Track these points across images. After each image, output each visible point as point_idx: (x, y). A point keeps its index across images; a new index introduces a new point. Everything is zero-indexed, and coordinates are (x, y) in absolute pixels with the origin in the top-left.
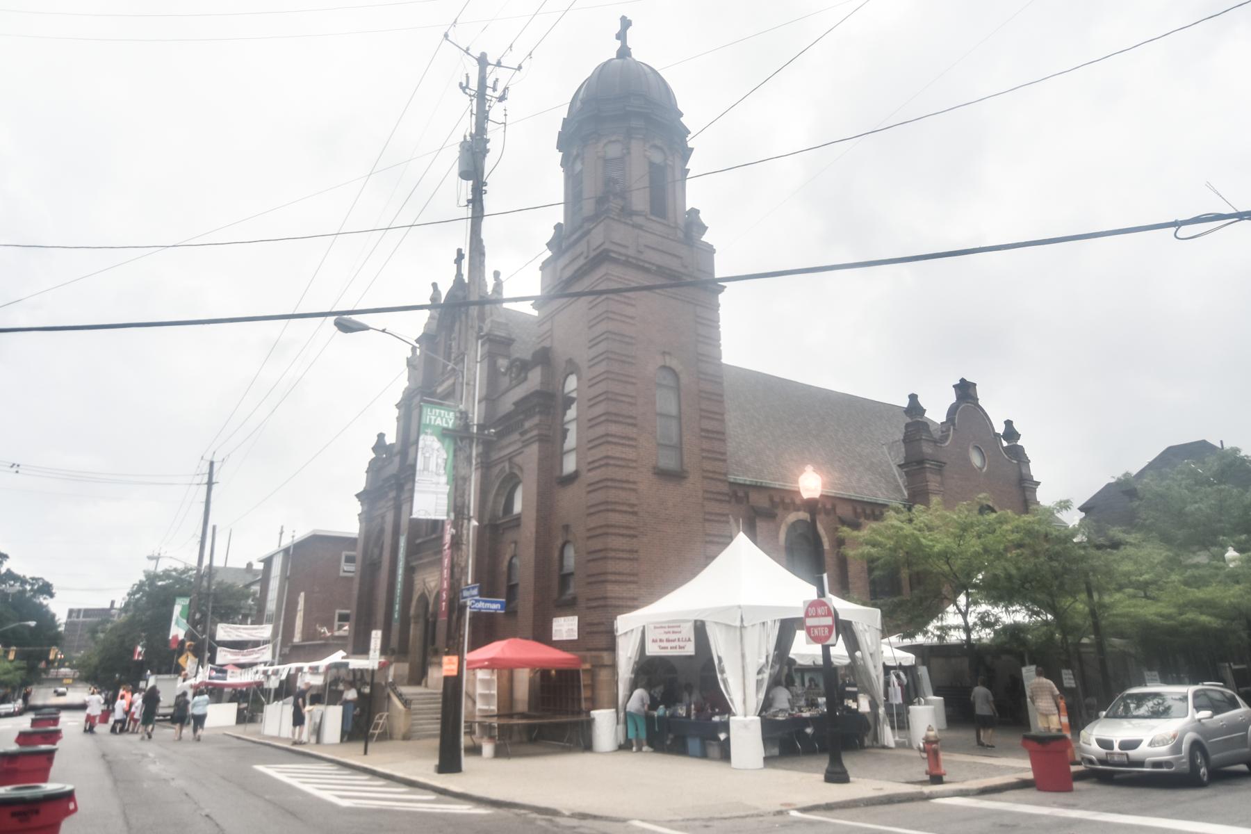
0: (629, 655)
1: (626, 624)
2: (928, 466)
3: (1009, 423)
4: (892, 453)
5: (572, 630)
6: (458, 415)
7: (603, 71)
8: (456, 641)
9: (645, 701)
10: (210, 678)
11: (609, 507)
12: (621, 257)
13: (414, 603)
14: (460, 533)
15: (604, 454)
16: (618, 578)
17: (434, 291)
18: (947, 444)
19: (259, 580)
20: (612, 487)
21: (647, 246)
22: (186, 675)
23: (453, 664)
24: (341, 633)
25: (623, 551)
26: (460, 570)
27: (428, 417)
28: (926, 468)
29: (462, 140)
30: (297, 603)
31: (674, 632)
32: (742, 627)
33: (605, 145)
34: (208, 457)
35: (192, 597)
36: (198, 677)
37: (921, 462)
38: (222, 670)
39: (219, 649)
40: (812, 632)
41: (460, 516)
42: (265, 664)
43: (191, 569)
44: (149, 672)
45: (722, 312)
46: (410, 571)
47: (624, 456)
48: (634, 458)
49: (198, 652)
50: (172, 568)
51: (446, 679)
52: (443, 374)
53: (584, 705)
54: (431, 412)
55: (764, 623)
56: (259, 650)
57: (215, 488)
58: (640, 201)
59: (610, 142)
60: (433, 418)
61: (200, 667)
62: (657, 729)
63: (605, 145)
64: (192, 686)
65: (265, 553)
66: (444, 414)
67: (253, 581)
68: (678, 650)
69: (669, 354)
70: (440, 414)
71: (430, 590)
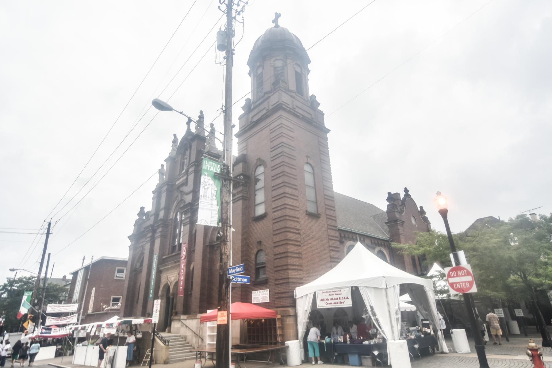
0: (306, 309)
1: (299, 291)
2: (399, 222)
3: (421, 207)
4: (376, 220)
5: (266, 297)
6: (222, 167)
7: (270, 32)
8: (226, 301)
9: (318, 335)
10: (41, 333)
11: (288, 230)
12: (287, 108)
13: (161, 289)
14: (225, 235)
15: (283, 203)
16: (293, 267)
17: (174, 138)
18: (403, 214)
19: (70, 284)
20: (288, 220)
21: (297, 106)
22: (27, 332)
23: (224, 316)
24: (116, 307)
25: (295, 253)
26: (226, 257)
27: (206, 165)
28: (398, 223)
29: (219, 30)
30: (91, 293)
31: (336, 294)
32: (387, 288)
33: (275, 61)
34: (48, 221)
35: (34, 291)
36: (35, 332)
37: (396, 221)
38: (49, 329)
39: (47, 317)
40: (455, 286)
41: (226, 225)
42: (73, 324)
43: (34, 277)
44: (5, 332)
45: (329, 141)
46: (159, 272)
47: (293, 204)
48: (297, 206)
49: (35, 320)
50: (23, 277)
51: (219, 327)
52: (179, 175)
53: (279, 339)
54: (208, 163)
55: (394, 286)
56: (70, 317)
57: (50, 236)
58: (292, 86)
59: (277, 60)
60: (209, 166)
61: (36, 327)
62: (325, 350)
63: (275, 61)
64: (30, 338)
65: (74, 270)
66: (215, 165)
67: (65, 284)
68: (339, 304)
69: (309, 157)
70: (212, 165)
71: (171, 281)
